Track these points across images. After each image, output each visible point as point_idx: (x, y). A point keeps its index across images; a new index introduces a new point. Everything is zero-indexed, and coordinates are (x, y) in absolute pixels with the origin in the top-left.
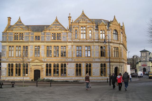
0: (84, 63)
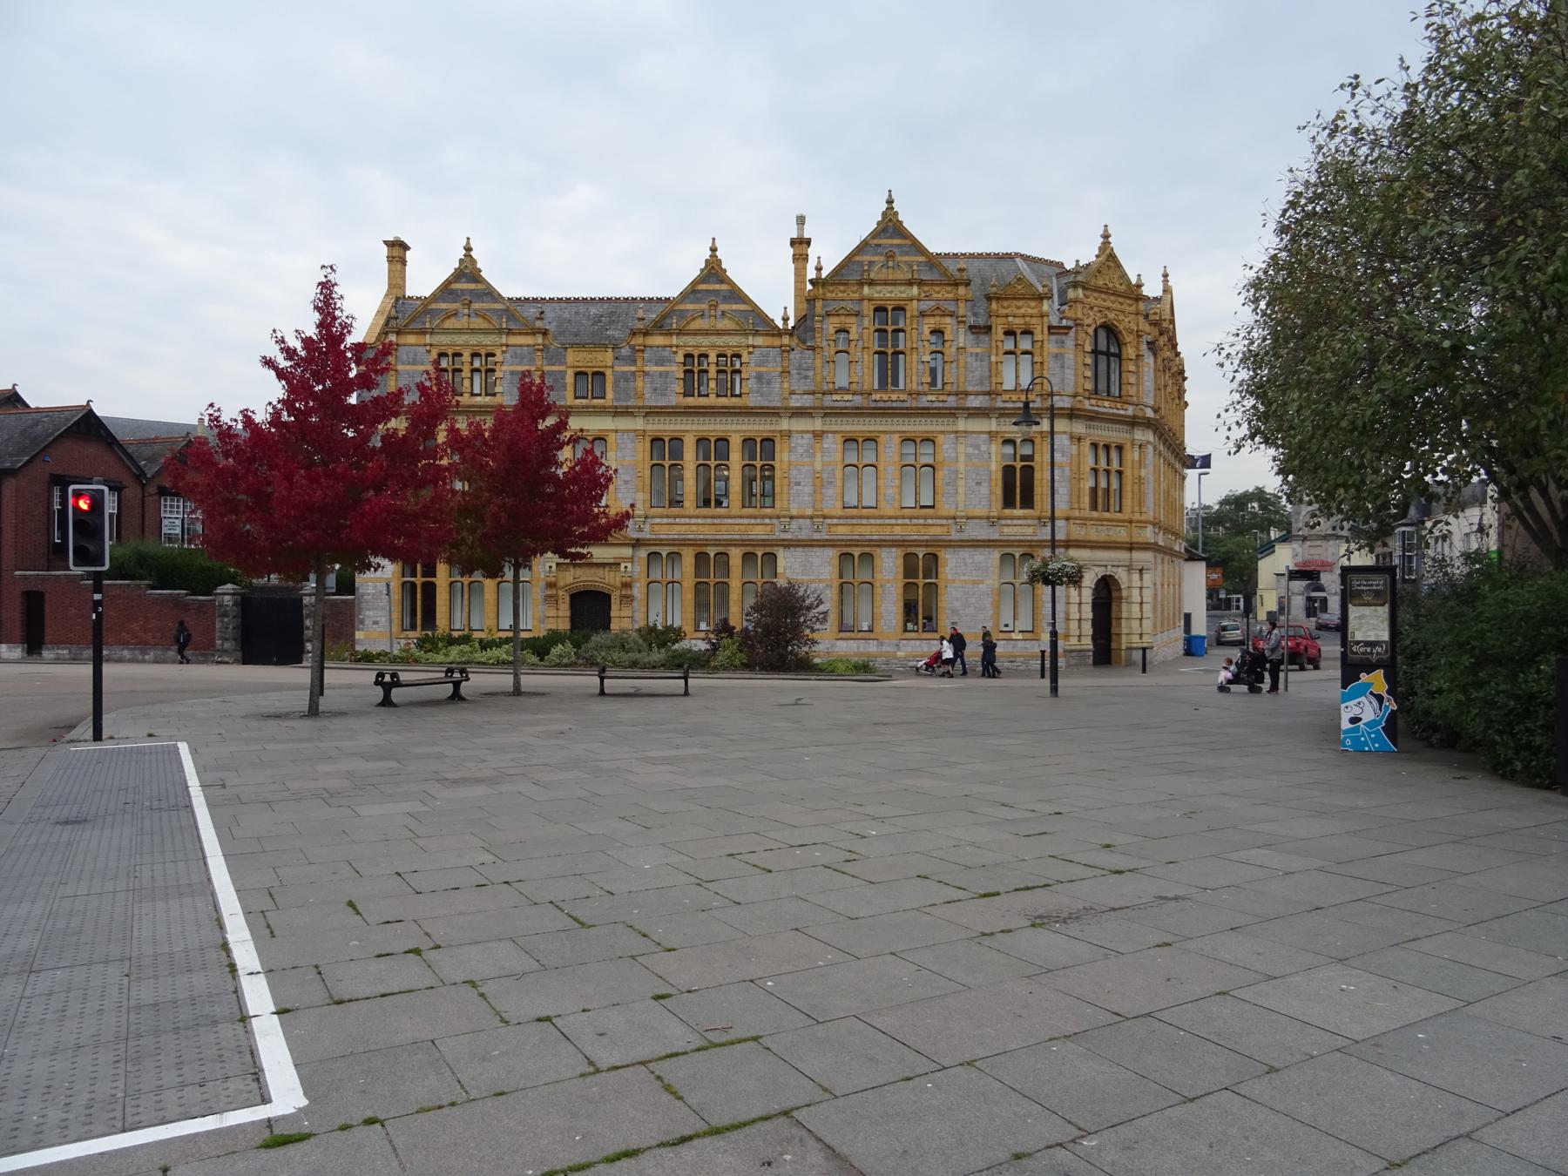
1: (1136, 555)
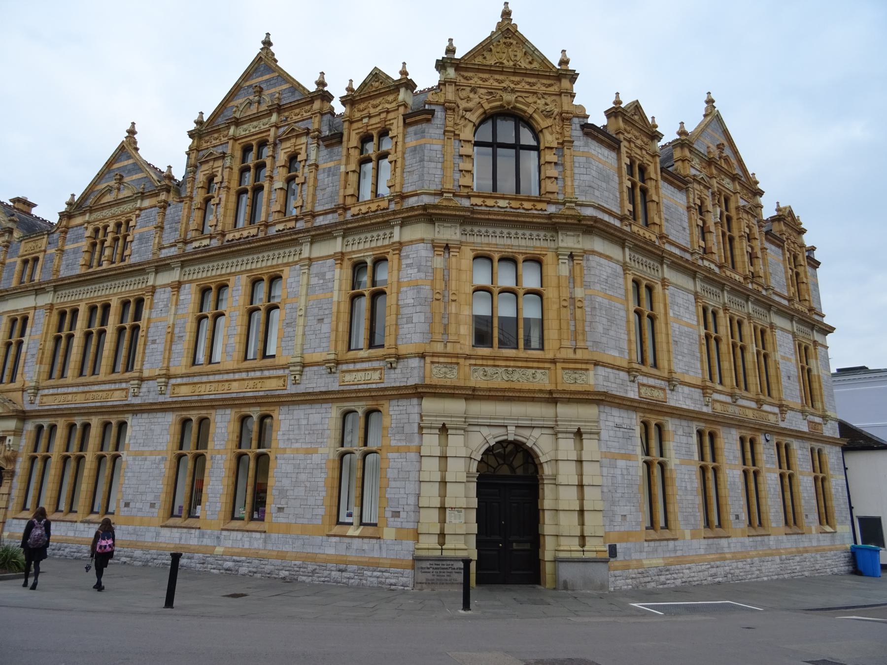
0: (228, 411)
1: (563, 410)
